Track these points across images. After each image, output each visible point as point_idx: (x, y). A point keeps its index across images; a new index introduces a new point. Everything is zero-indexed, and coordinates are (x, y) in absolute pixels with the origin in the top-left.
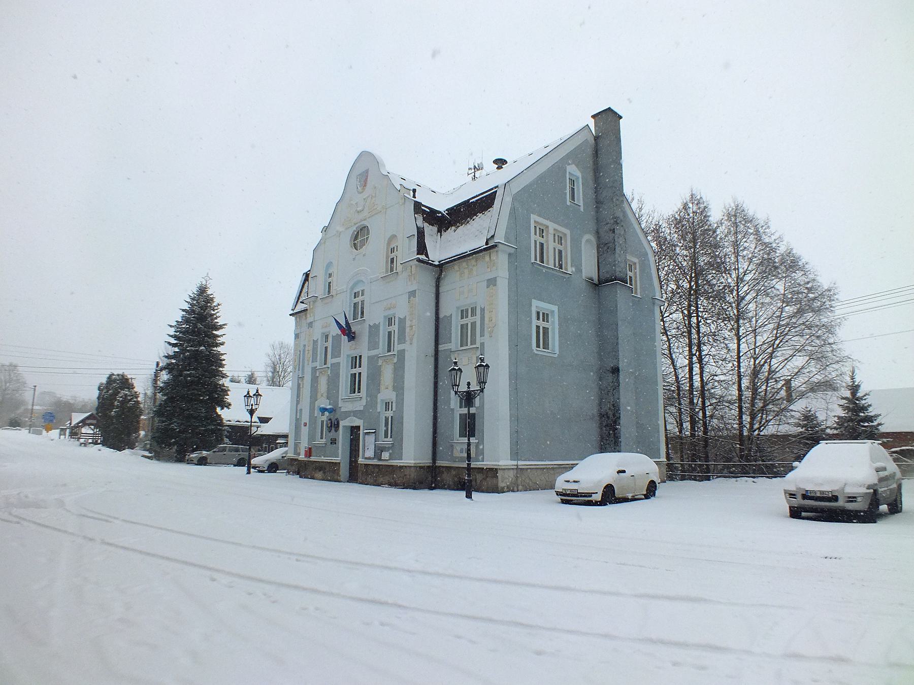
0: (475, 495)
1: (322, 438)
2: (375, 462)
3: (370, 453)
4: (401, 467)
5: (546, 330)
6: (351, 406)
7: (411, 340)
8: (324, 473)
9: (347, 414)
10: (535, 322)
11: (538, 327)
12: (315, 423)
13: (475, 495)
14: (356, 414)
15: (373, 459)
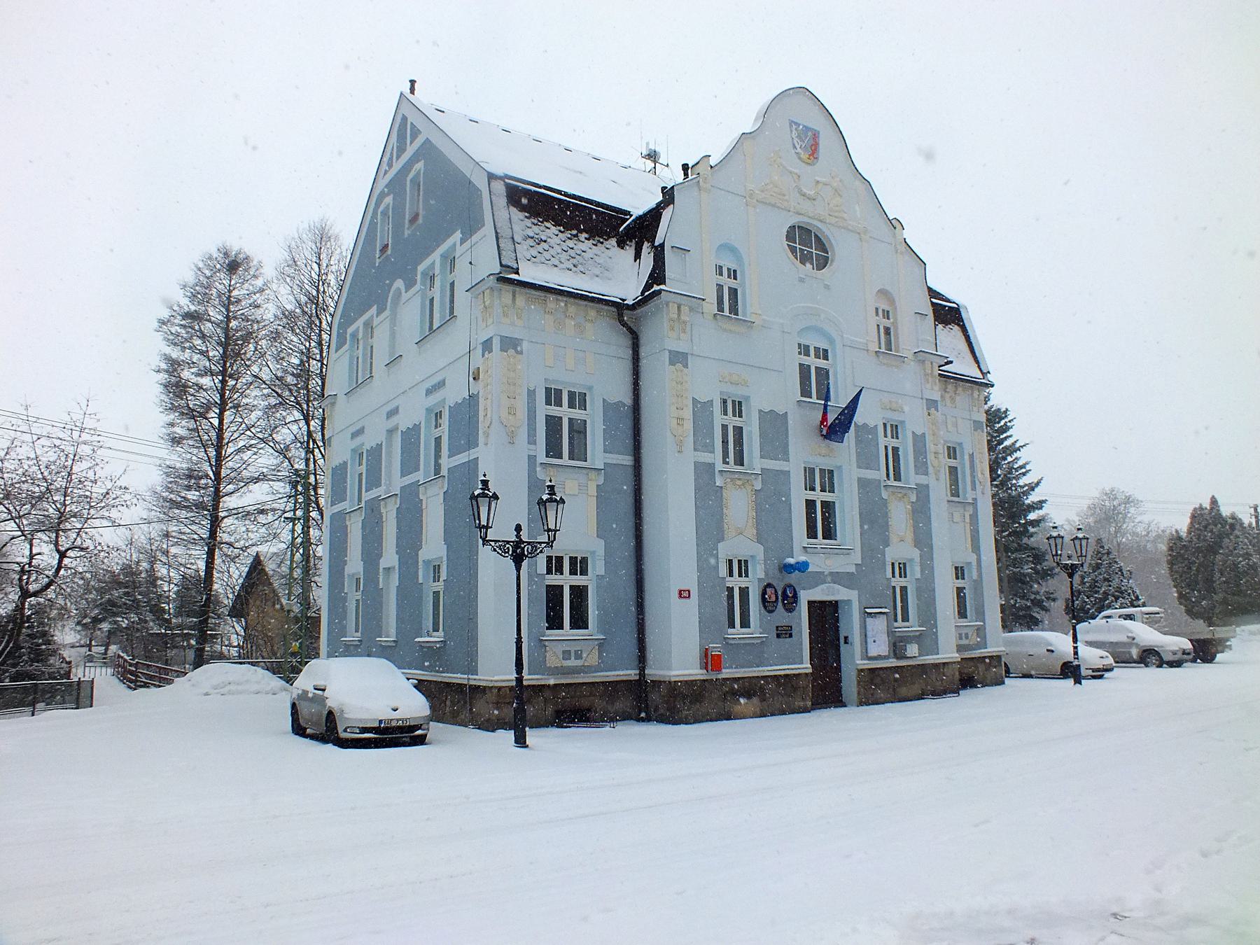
0: (532, 736)
1: (436, 629)
2: (893, 662)
3: (880, 646)
4: (936, 666)
5: (739, 431)
6: (830, 569)
7: (487, 435)
8: (763, 700)
9: (819, 579)
10: (882, 441)
11: (725, 427)
12: (419, 600)
13: (532, 736)
14: (837, 578)
15: (885, 658)
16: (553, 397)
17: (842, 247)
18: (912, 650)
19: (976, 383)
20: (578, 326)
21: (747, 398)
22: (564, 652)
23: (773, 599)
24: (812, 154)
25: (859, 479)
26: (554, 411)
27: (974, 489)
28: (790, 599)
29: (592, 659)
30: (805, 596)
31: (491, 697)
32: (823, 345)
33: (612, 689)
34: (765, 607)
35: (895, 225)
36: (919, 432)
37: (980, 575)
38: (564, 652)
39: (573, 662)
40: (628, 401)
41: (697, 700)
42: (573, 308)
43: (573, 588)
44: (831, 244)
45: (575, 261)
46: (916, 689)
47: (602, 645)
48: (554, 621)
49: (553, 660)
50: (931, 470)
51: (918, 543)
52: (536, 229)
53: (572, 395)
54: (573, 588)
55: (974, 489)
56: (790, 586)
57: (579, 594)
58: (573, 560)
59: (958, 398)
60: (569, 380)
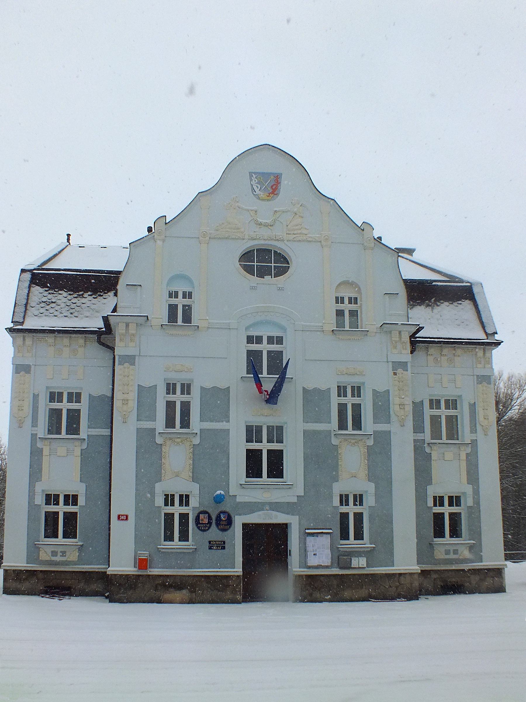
2: (336, 571)
16: (55, 397)
17: (299, 256)
18: (356, 562)
19: (483, 344)
20: (436, 359)
21: (363, 383)
22: (52, 552)
23: (206, 521)
24: (273, 193)
25: (305, 432)
26: (435, 412)
27: (473, 430)
28: (225, 522)
29: (73, 556)
30: (239, 522)
31: (370, 576)
32: (275, 333)
33: (87, 576)
34: (198, 528)
35: (365, 228)
36: (381, 389)
37: (477, 502)
38: (52, 552)
39: (58, 558)
40: (109, 394)
41: (131, 588)
42: (66, 340)
43: (451, 514)
44: (289, 257)
45: (72, 311)
46: (364, 592)
47: (81, 548)
48: (439, 533)
49: (44, 556)
50: (393, 418)
51: (371, 477)
52: (50, 296)
53: (447, 402)
54: (451, 514)
55: (473, 430)
56: (224, 512)
57: (359, 517)
58: (451, 498)
59: (457, 359)
60: (65, 384)
